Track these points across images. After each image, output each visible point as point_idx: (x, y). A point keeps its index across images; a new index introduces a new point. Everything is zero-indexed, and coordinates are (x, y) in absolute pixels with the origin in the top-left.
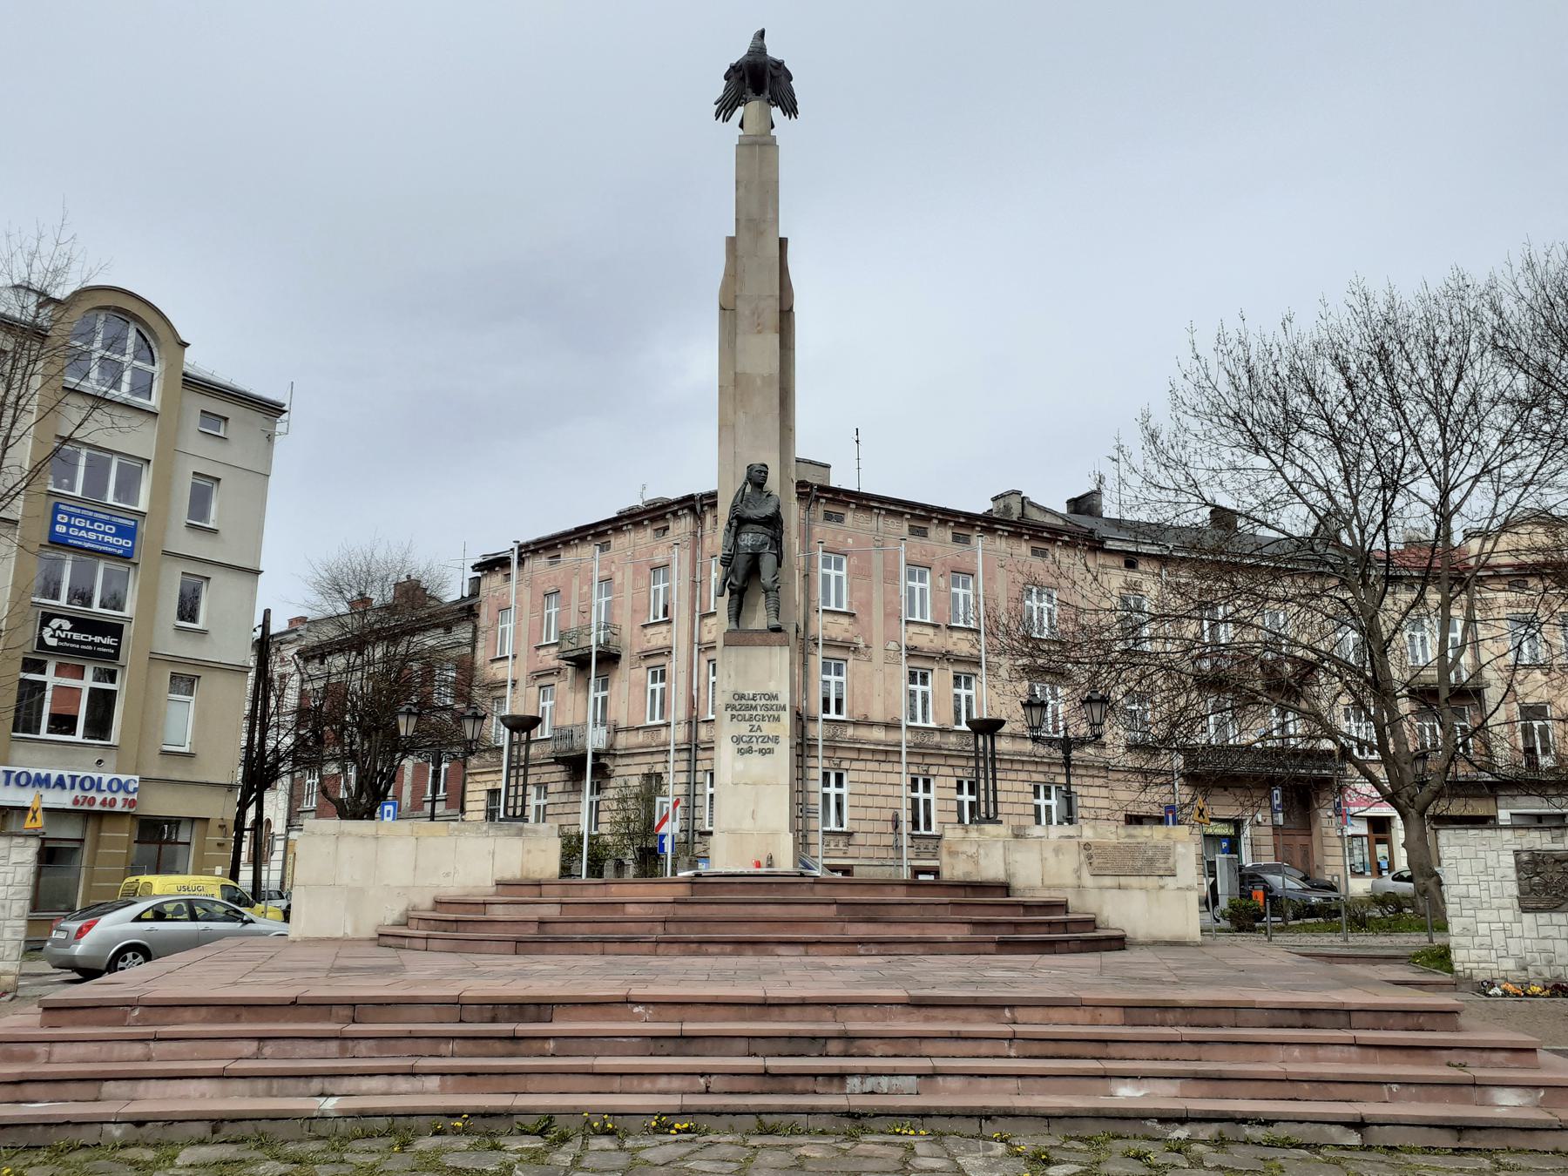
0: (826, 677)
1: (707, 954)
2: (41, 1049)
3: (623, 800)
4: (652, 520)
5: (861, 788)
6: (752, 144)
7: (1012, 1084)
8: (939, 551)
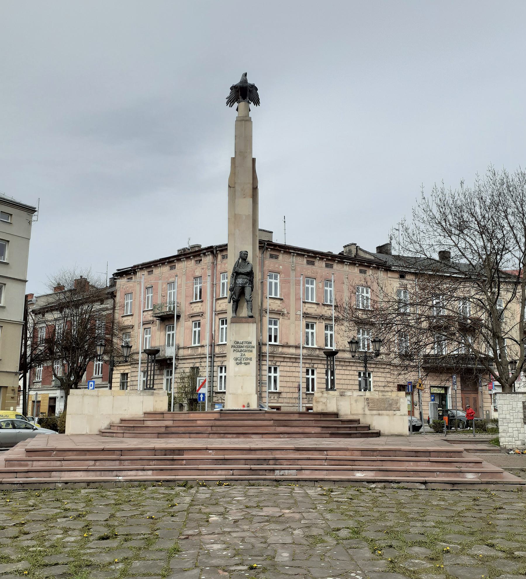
0: (270, 326)
1: (227, 438)
2: (30, 463)
3: (182, 378)
4: (194, 256)
5: (285, 374)
7: (325, 472)
8: (319, 271)
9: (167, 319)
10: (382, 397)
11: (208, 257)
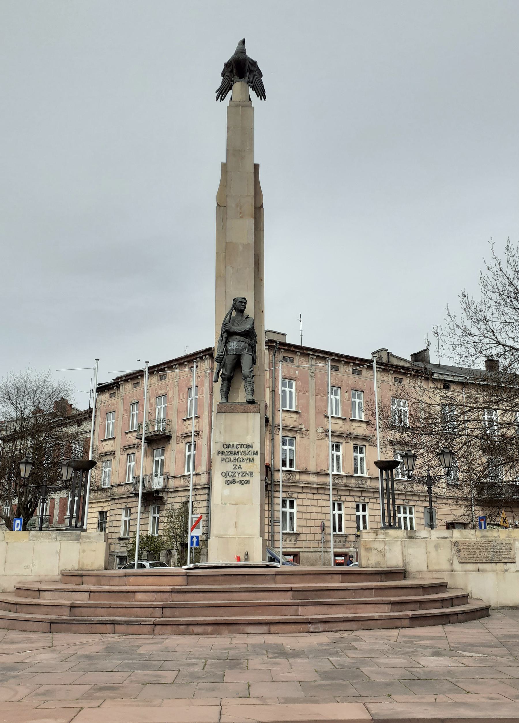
1: (193, 633)
3: (171, 516)
5: (303, 509)
6: (237, 106)
8: (345, 378)
9: (158, 441)
10: (482, 539)
11: (206, 362)
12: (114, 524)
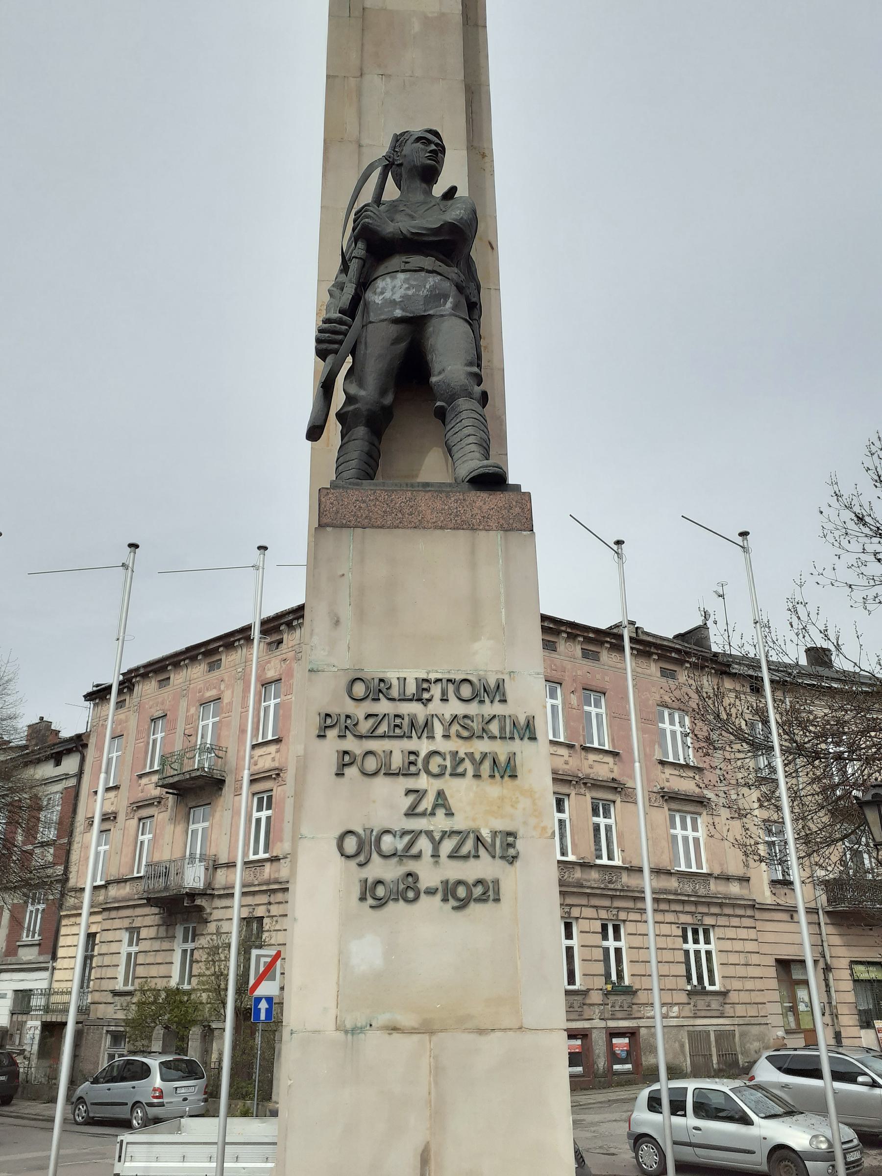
8: (569, 665)
9: (195, 790)
12: (107, 960)
